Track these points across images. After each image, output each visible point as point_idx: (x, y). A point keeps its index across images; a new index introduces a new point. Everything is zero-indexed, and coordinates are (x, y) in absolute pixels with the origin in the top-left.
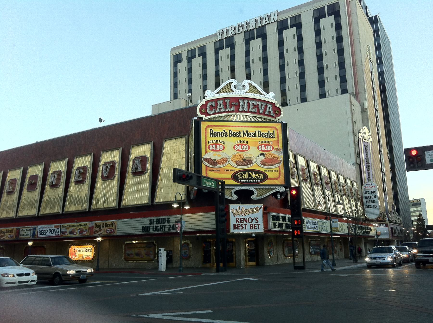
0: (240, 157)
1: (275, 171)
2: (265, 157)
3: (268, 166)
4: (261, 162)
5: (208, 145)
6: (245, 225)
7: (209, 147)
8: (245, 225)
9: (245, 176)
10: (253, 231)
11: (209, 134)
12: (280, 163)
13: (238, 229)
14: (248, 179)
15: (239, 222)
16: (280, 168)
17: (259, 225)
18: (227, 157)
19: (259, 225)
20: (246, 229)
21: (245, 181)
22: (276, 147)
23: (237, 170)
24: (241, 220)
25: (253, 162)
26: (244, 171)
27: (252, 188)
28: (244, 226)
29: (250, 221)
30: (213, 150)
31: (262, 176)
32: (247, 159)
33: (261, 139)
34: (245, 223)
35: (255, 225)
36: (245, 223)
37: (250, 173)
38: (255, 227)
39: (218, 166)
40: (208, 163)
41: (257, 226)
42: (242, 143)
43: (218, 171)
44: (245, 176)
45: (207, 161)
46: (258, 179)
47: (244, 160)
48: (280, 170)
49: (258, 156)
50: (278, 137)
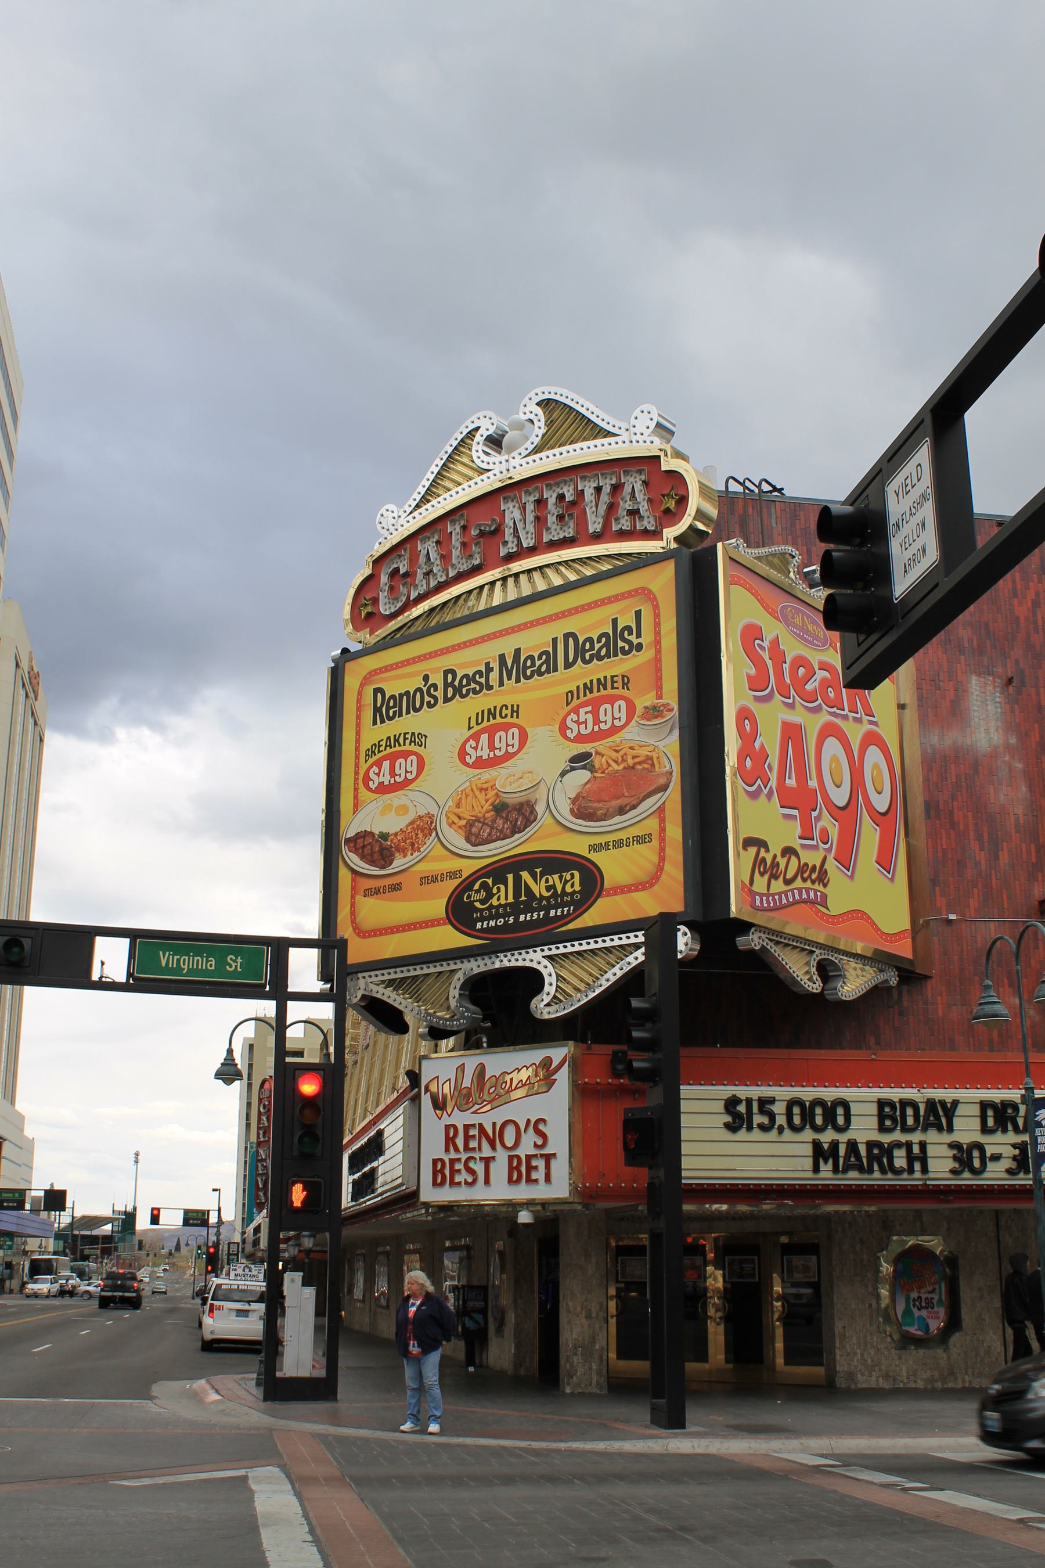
0: (481, 797)
1: (640, 840)
2: (592, 769)
3: (604, 818)
4: (574, 801)
6: (487, 1161)
7: (367, 779)
8: (487, 1161)
9: (504, 895)
10: (522, 1192)
11: (368, 714)
12: (664, 788)
13: (453, 1184)
14: (515, 908)
16: (662, 820)
17: (548, 1158)
18: (434, 811)
19: (548, 1158)
20: (487, 1181)
21: (501, 922)
22: (644, 701)
23: (469, 867)
24: (467, 1138)
25: (540, 808)
27: (534, 958)
28: (479, 1168)
29: (509, 1141)
30: (382, 789)
32: (512, 800)
34: (487, 1152)
36: (487, 1152)
37: (525, 875)
38: (530, 1168)
40: (363, 857)
41: (540, 1163)
42: (492, 723)
44: (504, 895)
45: (355, 851)
46: (557, 899)
47: (500, 808)
48: (662, 830)
49: (563, 774)
50: (657, 642)
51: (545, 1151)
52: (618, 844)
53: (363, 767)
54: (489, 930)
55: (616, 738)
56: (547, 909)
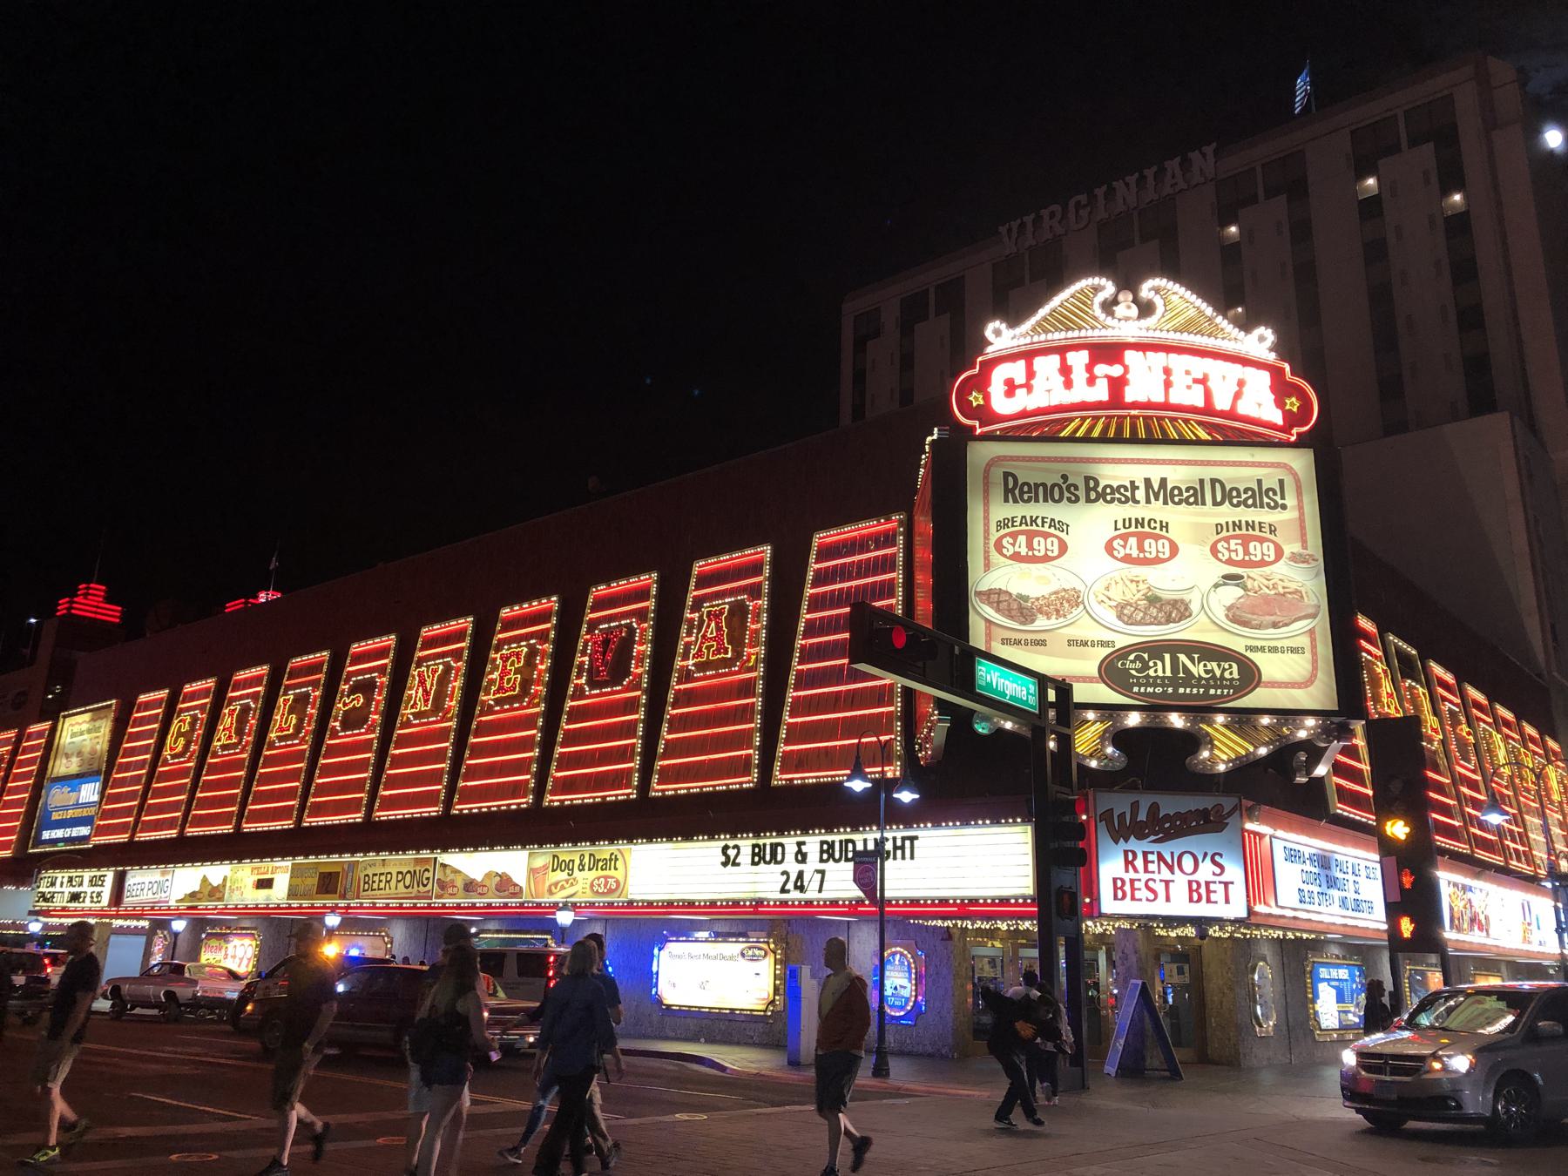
1: (1294, 650)
2: (1245, 588)
3: (1259, 627)
5: (994, 536)
7: (999, 546)
9: (1161, 668)
14: (1174, 681)
15: (1136, 871)
23: (1122, 642)
26: (1156, 649)
30: (1016, 557)
31: (1234, 672)
32: (1166, 596)
33: (1227, 513)
35: (1207, 884)
39: (1041, 622)
40: (998, 610)
43: (1042, 643)
44: (1161, 668)
46: (1219, 682)
47: (1153, 600)
49: (1216, 586)
51: (1222, 878)
52: (1273, 650)
53: (994, 536)
54: (1145, 694)
55: (1267, 570)
56: (1207, 687)
